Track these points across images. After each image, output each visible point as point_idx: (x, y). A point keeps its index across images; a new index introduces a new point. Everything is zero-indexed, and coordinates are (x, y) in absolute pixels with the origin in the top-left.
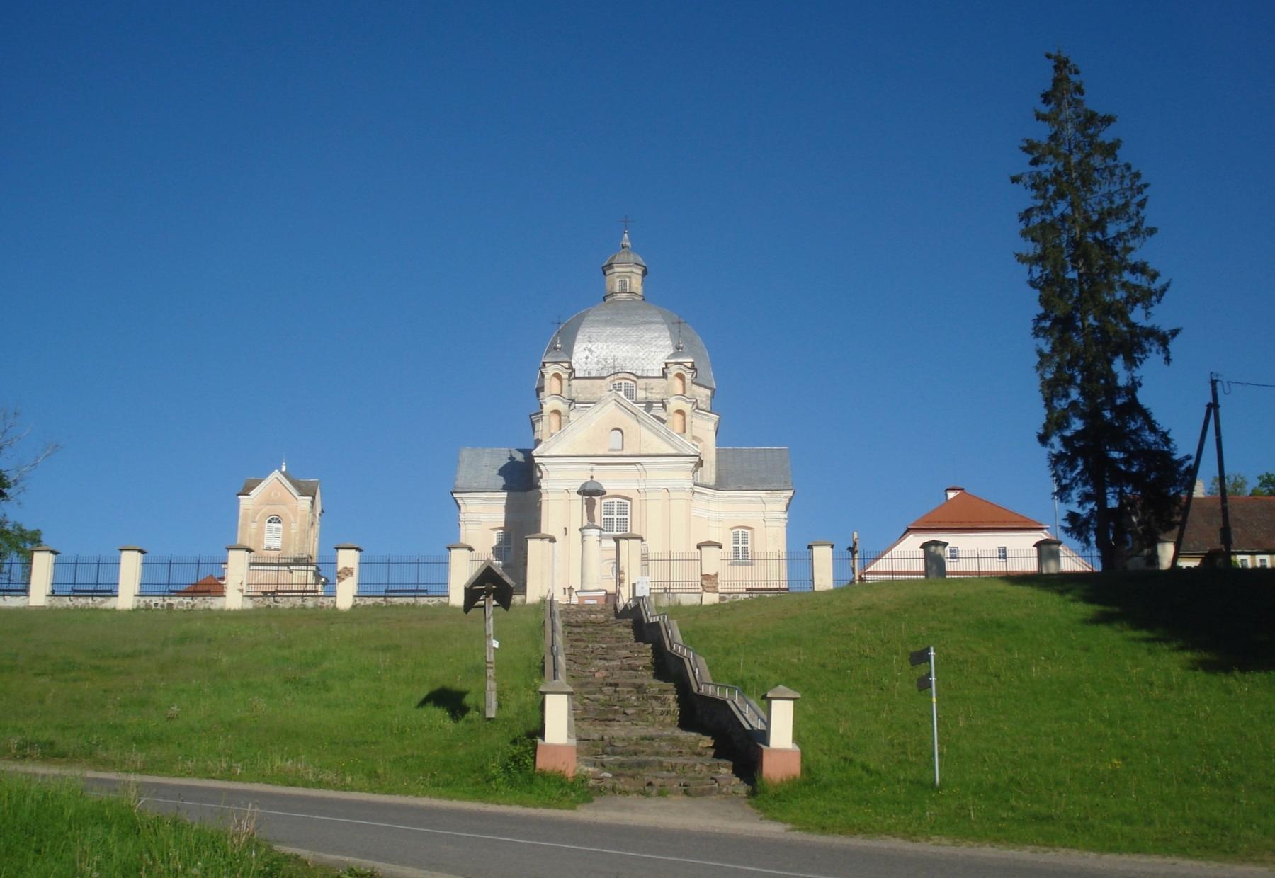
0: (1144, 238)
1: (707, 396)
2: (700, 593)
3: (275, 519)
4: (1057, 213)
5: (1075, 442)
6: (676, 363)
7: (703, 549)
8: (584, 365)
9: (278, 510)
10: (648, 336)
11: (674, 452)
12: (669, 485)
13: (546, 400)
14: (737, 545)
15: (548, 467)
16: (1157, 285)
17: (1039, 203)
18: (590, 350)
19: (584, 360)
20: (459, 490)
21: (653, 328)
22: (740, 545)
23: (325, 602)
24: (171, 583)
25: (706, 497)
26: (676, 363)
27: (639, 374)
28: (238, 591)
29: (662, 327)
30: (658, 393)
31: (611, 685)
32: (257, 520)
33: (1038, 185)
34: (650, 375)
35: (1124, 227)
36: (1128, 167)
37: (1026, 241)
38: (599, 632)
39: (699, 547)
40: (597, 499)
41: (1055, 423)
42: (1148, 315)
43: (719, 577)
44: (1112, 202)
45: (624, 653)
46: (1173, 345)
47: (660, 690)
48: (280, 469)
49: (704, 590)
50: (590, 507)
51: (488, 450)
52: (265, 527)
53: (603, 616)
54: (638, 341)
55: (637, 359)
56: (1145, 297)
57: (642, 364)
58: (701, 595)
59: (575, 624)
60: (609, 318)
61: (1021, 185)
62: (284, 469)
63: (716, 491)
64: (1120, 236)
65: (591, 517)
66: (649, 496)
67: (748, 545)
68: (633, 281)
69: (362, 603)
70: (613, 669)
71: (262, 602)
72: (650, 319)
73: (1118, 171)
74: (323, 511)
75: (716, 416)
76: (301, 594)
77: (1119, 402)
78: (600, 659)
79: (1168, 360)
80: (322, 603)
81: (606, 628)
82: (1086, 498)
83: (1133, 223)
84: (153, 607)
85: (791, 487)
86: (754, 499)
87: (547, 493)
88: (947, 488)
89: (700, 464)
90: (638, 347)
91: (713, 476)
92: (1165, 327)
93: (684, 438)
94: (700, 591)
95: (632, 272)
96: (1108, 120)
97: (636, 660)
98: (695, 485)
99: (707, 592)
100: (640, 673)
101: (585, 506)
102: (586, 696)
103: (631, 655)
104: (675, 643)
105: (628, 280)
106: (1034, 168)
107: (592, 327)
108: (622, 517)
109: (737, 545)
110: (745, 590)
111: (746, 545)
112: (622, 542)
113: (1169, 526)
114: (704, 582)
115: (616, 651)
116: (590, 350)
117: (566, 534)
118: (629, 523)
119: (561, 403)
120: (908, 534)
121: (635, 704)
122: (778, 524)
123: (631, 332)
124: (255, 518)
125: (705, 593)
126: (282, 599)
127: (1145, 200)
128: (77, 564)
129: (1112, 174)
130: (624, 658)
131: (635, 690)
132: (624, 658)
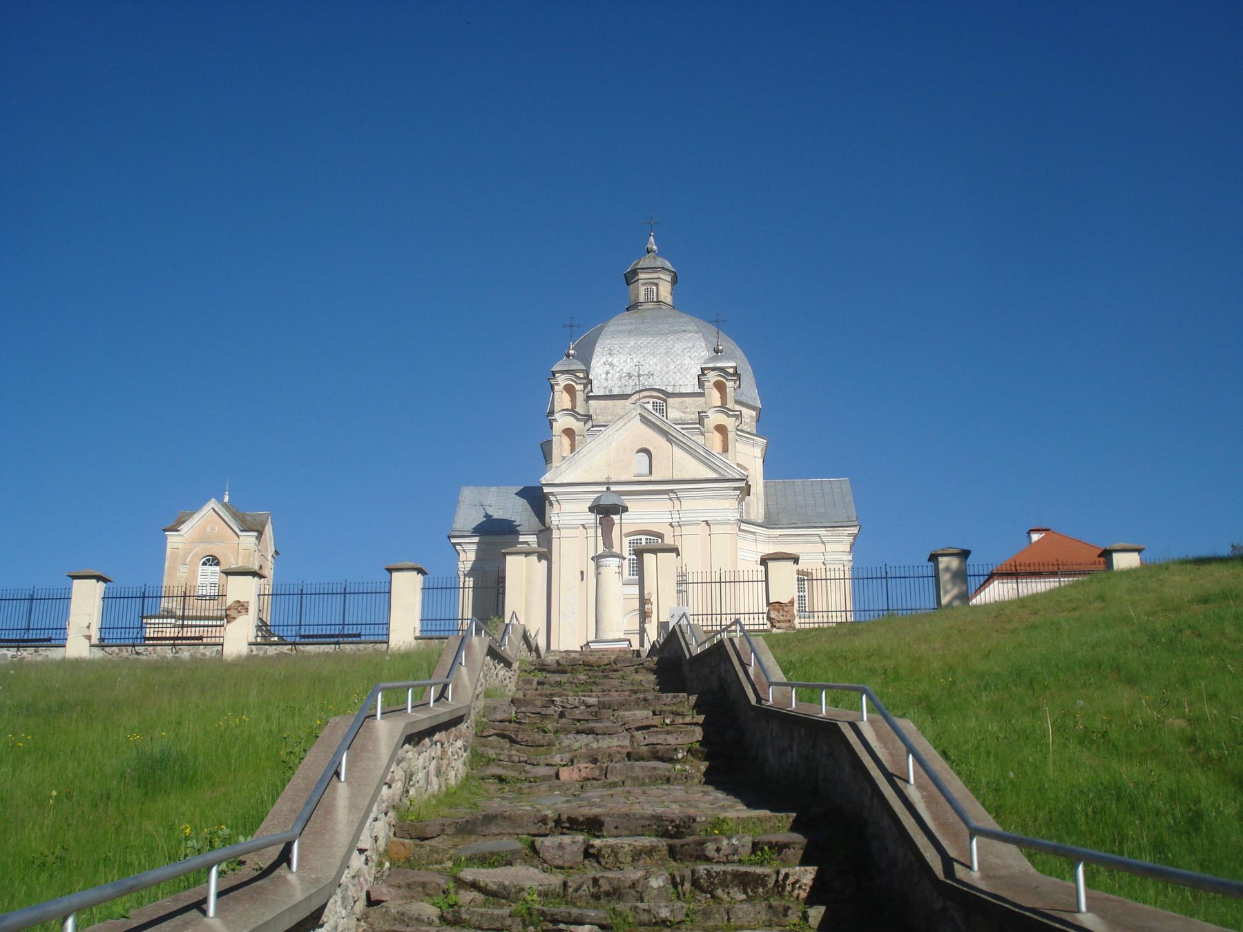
1: (751, 417)
6: (714, 369)
7: (771, 564)
8: (603, 381)
9: (215, 550)
10: (678, 347)
11: (714, 475)
12: (708, 516)
13: (557, 416)
15: (559, 497)
18: (611, 364)
19: (604, 376)
20: (457, 534)
21: (685, 337)
23: (208, 653)
25: (752, 536)
26: (714, 369)
27: (670, 390)
28: (83, 639)
29: (696, 336)
31: (573, 825)
32: (188, 561)
34: (683, 390)
38: (597, 680)
39: (764, 561)
45: (640, 715)
47: (756, 846)
48: (220, 500)
51: (493, 489)
52: (198, 571)
54: (667, 352)
55: (667, 373)
57: (674, 379)
59: (554, 666)
60: (633, 328)
62: (226, 499)
63: (766, 529)
65: (608, 543)
66: (685, 530)
68: (661, 288)
69: (261, 653)
70: (610, 757)
71: (117, 654)
74: (277, 552)
75: (763, 440)
76: (172, 642)
78: (578, 732)
80: (204, 654)
81: (611, 674)
85: (856, 523)
86: (812, 539)
87: (559, 529)
88: (1029, 529)
89: (747, 490)
91: (762, 511)
95: (659, 278)
97: (668, 733)
100: (678, 767)
102: (468, 874)
103: (657, 720)
104: (771, 684)
105: (655, 288)
107: (613, 337)
112: (649, 558)
114: (773, 615)
115: (621, 713)
116: (611, 364)
117: (582, 579)
120: (991, 580)
121: (664, 913)
123: (659, 342)
124: (186, 559)
126: (146, 650)
130: (638, 729)
131: (662, 843)
132: (638, 729)
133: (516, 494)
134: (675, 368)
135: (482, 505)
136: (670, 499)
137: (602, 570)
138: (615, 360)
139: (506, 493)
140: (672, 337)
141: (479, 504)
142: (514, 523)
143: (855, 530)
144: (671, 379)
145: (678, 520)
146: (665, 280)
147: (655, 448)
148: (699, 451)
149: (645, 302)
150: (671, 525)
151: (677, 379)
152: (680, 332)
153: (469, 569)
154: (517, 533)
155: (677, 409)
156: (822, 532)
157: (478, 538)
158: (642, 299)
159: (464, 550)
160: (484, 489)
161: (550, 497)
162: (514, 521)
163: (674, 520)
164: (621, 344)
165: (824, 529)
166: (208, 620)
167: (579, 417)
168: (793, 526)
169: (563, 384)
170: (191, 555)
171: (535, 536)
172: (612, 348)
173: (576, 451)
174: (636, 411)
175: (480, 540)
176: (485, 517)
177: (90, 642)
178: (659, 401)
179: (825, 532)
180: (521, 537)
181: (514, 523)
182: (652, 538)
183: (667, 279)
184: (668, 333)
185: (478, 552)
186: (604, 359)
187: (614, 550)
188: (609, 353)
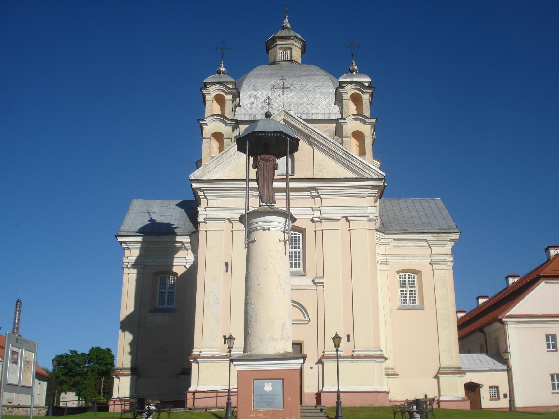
6: (351, 83)
8: (248, 110)
10: (311, 85)
11: (353, 176)
13: (207, 120)
14: (404, 289)
15: (207, 193)
18: (255, 97)
19: (249, 105)
21: (316, 79)
22: (408, 289)
26: (351, 83)
29: (325, 78)
34: (315, 117)
51: (158, 201)
55: (301, 104)
63: (382, 234)
66: (326, 225)
67: (416, 289)
68: (294, 52)
72: (313, 73)
75: (378, 163)
85: (457, 231)
86: (420, 243)
87: (206, 222)
90: (303, 94)
95: (292, 44)
107: (257, 78)
109: (404, 289)
111: (413, 289)
116: (255, 97)
117: (227, 270)
118: (301, 258)
119: (222, 125)
122: (445, 267)
123: (295, 82)
133: (176, 205)
134: (308, 100)
135: (148, 212)
136: (312, 196)
137: (256, 235)
138: (259, 94)
139: (168, 205)
140: (305, 78)
141: (146, 211)
142: (173, 226)
143: (456, 236)
144: (305, 109)
145: (319, 216)
146: (297, 47)
148: (339, 153)
149: (281, 61)
150: (312, 220)
151: (310, 109)
152: (311, 75)
153: (132, 263)
154: (175, 234)
156: (429, 237)
157: (142, 237)
158: (279, 58)
159: (128, 248)
160: (151, 202)
161: (198, 192)
162: (173, 225)
163: (315, 216)
164: (264, 82)
165: (431, 235)
167: (228, 122)
168: (405, 232)
169: (213, 94)
171: (188, 237)
172: (256, 86)
173: (224, 152)
174: (280, 116)
175: (143, 239)
176: (149, 221)
179: (432, 238)
180: (178, 237)
181: (173, 226)
182: (297, 233)
183: (299, 46)
184: (302, 76)
185: (142, 249)
186: (250, 93)
187: (276, 206)
188: (254, 89)
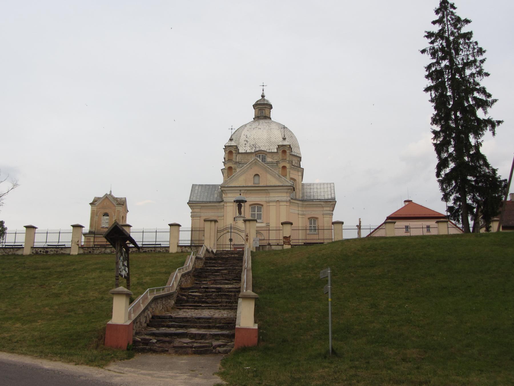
0: (483, 77)
2: (281, 245)
3: (106, 214)
4: (443, 65)
5: (454, 155)
11: (281, 184)
16: (490, 99)
17: (434, 61)
19: (244, 145)
24: (6, 242)
28: (76, 245)
30: (276, 159)
32: (98, 215)
33: (434, 54)
35: (474, 70)
36: (476, 43)
37: (428, 80)
40: (243, 204)
41: (442, 164)
42: (486, 113)
43: (291, 238)
44: (468, 59)
46: (497, 129)
49: (284, 243)
50: (240, 207)
53: (237, 255)
56: (484, 104)
58: (283, 246)
61: (426, 53)
64: (472, 75)
71: (87, 250)
73: (471, 45)
77: (471, 153)
79: (494, 134)
82: (456, 200)
83: (478, 69)
84: (39, 252)
86: (319, 206)
92: (495, 119)
93: (286, 178)
94: (282, 244)
96: (467, 21)
98: (292, 199)
99: (286, 244)
101: (237, 207)
106: (432, 45)
108: (259, 213)
109: (311, 225)
110: (303, 244)
113: (495, 214)
125: (284, 245)
127: (484, 60)
128: (16, 233)
129: (469, 46)
147: (261, 174)
155: (271, 158)
166: (99, 235)
170: (99, 213)
172: (247, 135)
177: (79, 246)
178: (264, 155)
